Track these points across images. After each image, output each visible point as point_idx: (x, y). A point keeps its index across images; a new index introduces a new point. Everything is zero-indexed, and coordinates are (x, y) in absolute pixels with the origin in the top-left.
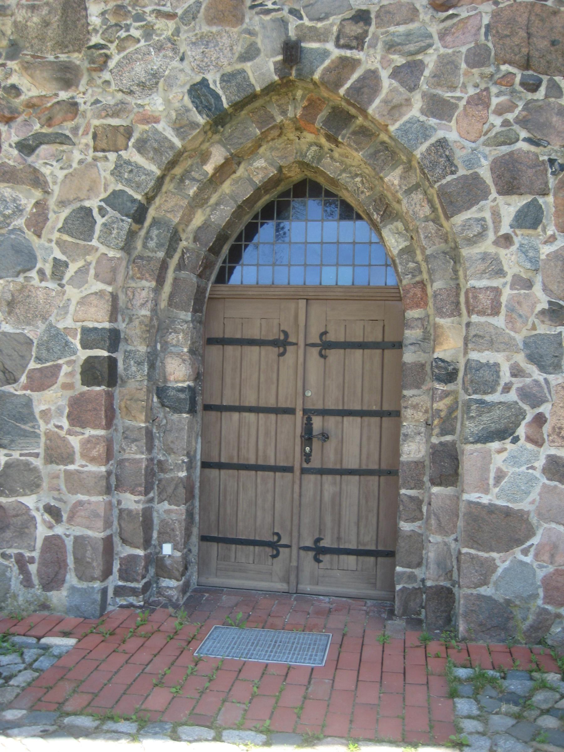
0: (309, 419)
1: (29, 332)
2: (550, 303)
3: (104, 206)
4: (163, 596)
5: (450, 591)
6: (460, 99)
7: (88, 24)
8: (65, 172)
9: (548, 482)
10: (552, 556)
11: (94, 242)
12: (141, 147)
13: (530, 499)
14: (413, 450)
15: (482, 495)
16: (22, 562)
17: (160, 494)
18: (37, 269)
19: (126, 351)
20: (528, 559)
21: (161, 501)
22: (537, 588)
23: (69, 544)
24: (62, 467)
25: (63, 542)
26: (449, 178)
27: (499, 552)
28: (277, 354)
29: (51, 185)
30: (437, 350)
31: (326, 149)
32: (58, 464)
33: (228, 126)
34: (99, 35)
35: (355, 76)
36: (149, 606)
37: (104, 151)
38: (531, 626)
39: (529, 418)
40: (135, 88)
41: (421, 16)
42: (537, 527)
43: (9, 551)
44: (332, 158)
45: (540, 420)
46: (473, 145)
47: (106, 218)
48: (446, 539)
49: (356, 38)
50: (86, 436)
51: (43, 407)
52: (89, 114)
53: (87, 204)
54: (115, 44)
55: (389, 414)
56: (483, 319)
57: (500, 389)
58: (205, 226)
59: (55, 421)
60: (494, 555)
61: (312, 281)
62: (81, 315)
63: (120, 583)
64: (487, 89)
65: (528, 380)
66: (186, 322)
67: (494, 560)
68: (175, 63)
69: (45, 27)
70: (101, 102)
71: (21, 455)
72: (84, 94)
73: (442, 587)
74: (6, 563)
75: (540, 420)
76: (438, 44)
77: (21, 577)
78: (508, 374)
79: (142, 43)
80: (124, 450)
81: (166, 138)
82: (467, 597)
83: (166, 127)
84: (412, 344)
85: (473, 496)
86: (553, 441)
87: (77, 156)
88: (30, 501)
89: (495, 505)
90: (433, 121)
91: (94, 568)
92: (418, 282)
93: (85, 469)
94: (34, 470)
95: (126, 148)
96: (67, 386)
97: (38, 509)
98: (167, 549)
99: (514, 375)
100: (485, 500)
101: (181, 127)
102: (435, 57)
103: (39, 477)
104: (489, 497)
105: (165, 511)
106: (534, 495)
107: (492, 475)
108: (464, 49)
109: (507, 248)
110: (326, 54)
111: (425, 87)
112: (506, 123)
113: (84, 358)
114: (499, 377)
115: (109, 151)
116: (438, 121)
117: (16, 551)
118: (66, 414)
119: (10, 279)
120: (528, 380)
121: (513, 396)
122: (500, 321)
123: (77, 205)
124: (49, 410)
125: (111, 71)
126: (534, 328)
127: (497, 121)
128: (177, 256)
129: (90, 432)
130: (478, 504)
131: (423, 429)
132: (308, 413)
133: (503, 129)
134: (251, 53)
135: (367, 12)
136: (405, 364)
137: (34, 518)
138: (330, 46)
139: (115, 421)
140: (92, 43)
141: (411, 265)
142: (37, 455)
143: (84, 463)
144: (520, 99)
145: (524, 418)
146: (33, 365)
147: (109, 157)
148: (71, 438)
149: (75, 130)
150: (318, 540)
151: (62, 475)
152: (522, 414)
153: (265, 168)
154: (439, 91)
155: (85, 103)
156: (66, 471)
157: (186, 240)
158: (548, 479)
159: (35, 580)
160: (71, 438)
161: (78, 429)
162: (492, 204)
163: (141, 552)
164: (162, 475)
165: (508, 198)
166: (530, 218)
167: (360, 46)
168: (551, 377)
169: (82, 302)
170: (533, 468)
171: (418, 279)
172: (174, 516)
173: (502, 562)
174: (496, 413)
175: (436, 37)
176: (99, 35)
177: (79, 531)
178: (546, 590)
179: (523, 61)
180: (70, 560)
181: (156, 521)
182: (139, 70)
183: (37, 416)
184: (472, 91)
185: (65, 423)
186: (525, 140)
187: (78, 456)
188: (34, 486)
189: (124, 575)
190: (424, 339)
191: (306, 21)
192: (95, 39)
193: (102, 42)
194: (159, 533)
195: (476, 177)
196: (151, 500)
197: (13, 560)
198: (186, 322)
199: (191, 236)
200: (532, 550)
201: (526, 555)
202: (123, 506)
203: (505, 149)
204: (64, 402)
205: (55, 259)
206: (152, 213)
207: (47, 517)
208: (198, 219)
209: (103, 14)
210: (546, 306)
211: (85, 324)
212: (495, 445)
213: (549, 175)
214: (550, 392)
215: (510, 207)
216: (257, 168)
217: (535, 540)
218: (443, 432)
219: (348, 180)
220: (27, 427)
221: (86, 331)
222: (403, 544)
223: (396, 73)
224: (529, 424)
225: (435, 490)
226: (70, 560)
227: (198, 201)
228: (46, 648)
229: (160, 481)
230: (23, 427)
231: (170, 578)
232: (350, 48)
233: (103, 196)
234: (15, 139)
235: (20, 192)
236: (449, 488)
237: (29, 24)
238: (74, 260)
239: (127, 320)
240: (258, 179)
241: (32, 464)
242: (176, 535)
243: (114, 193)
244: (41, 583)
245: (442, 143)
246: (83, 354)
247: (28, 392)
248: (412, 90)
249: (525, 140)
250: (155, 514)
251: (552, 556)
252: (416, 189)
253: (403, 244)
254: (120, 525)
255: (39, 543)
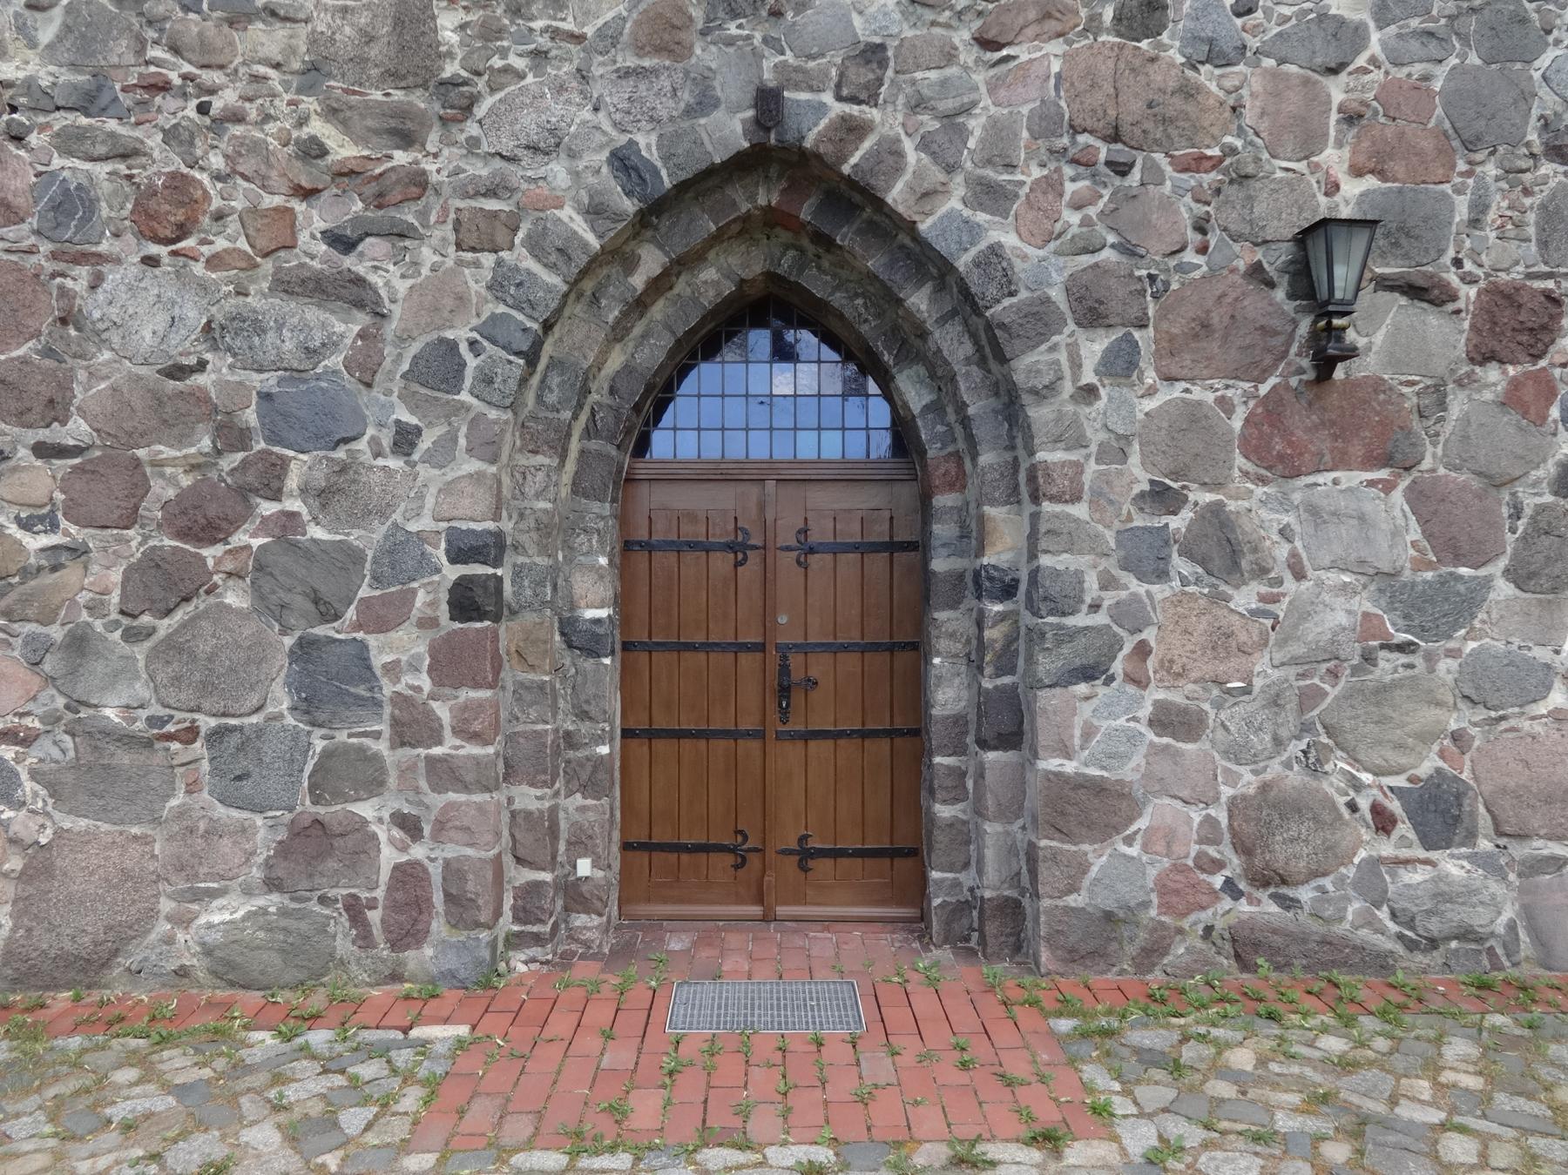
0: (785, 658)
1: (355, 537)
2: (1152, 482)
3: (479, 338)
4: (577, 941)
5: (1017, 904)
6: (1022, 183)
7: (439, 44)
8: (410, 282)
9: (1156, 739)
10: (1168, 845)
11: (464, 396)
12: (535, 246)
13: (1132, 764)
14: (948, 695)
15: (1065, 762)
16: (355, 910)
17: (568, 782)
18: (366, 438)
19: (515, 565)
20: (1133, 851)
21: (570, 794)
22: (1148, 894)
23: (435, 871)
24: (422, 752)
25: (425, 870)
26: (1007, 302)
27: (1092, 842)
28: (732, 562)
29: (386, 301)
30: (987, 552)
31: (810, 255)
32: (413, 746)
33: (666, 215)
34: (457, 62)
35: (867, 145)
36: (566, 960)
37: (473, 249)
38: (1143, 949)
39: (1127, 648)
40: (520, 152)
41: (962, 58)
42: (1144, 804)
43: (332, 893)
44: (819, 268)
45: (1142, 650)
46: (1041, 253)
47: (482, 357)
48: (1009, 828)
49: (866, 87)
50: (462, 699)
51: (388, 658)
52: (446, 191)
53: (450, 335)
54: (486, 77)
55: (905, 646)
56: (1058, 508)
57: (1085, 608)
58: (628, 369)
59: (408, 679)
60: (1086, 847)
61: (783, 452)
62: (446, 511)
63: (516, 928)
64: (1058, 170)
65: (1124, 594)
66: (603, 518)
67: (1086, 854)
68: (586, 114)
69: (367, 43)
70: (464, 171)
71: (350, 736)
72: (436, 156)
73: (1007, 899)
74: (327, 912)
75: (1142, 650)
76: (986, 101)
77: (354, 932)
78: (1096, 586)
79: (530, 79)
80: (517, 719)
81: (575, 233)
82: (1049, 911)
83: (575, 216)
84: (944, 545)
85: (1051, 764)
86: (1161, 680)
87: (428, 256)
88: (365, 810)
89: (1084, 775)
90: (981, 217)
91: (478, 908)
92: (950, 454)
93: (462, 752)
94: (376, 758)
95: (511, 247)
96: (428, 623)
97: (380, 820)
98: (584, 867)
99: (1103, 588)
100: (1070, 767)
101: (595, 211)
102: (983, 119)
103: (382, 770)
104: (1074, 764)
105: (577, 809)
106: (1138, 759)
107: (1077, 732)
108: (1025, 110)
109: (1090, 404)
110: (822, 108)
111: (969, 165)
112: (1086, 222)
113: (453, 577)
114: (1082, 590)
115: (482, 250)
116: (988, 217)
117: (345, 892)
118: (425, 668)
119: (321, 453)
120: (1124, 594)
121: (1101, 619)
122: (1080, 511)
123: (434, 336)
124: (398, 661)
125: (480, 122)
126: (1130, 519)
127: (1074, 218)
128: (584, 417)
129: (468, 694)
130: (1058, 775)
131: (963, 668)
132: (784, 651)
133: (1084, 229)
134: (705, 103)
135: (882, 47)
136: (934, 573)
137: (374, 837)
138: (828, 98)
139: (502, 675)
140: (446, 74)
141: (940, 428)
142: (377, 735)
143: (458, 742)
144: (1105, 185)
145: (1121, 649)
146: (364, 592)
147: (483, 260)
148: (434, 705)
149: (423, 215)
150: (803, 839)
151: (422, 765)
152: (1117, 644)
153: (718, 282)
154: (989, 173)
155: (438, 171)
156: (430, 760)
157: (598, 392)
158: (1157, 734)
159: (377, 931)
160: (434, 705)
161: (447, 691)
162: (1069, 341)
163: (547, 876)
164: (571, 754)
165: (1091, 333)
166: (1121, 364)
167: (872, 100)
168: (1155, 588)
169: (448, 489)
170: (1134, 719)
171: (950, 449)
172: (591, 816)
173: (1099, 860)
174: (1082, 641)
175: (983, 89)
176: (457, 62)
177: (451, 851)
178: (1161, 895)
179: (1111, 131)
180: (438, 898)
181: (563, 825)
182: (529, 123)
183: (378, 672)
184: (1037, 173)
185: (425, 682)
186: (1113, 246)
187: (447, 732)
188: (374, 785)
189: (521, 915)
190: (962, 537)
191: (789, 57)
192: (450, 69)
193: (464, 74)
194: (569, 843)
195: (1047, 300)
196: (557, 794)
197: (340, 905)
198: (603, 518)
199: (606, 386)
200: (1139, 837)
201: (1130, 845)
202: (517, 806)
203: (1086, 260)
204: (422, 648)
205: (398, 422)
206: (548, 349)
207: (397, 833)
208: (616, 361)
209: (463, 27)
210: (1147, 487)
211: (454, 524)
212: (1082, 688)
213: (1149, 298)
214: (1154, 609)
215: (1094, 347)
216: (706, 282)
217: (1142, 823)
218: (999, 673)
219: (844, 302)
220: (361, 691)
221: (453, 535)
222: (940, 838)
223: (924, 145)
224: (1128, 657)
225: (991, 756)
226: (438, 898)
227: (618, 333)
228: (424, 1043)
229: (568, 762)
230: (352, 690)
231: (588, 913)
232: (860, 102)
233: (475, 322)
234: (320, 225)
235: (333, 312)
236: (1010, 753)
237: (338, 37)
238: (430, 425)
239: (515, 516)
240: (709, 298)
241: (369, 748)
242: (596, 845)
243: (494, 317)
244: (387, 941)
245: (995, 251)
246: (452, 572)
247: (360, 635)
248: (950, 169)
249: (1113, 246)
250: (562, 815)
251: (1168, 845)
252: (952, 317)
253: (927, 398)
254: (512, 836)
255: (385, 876)
